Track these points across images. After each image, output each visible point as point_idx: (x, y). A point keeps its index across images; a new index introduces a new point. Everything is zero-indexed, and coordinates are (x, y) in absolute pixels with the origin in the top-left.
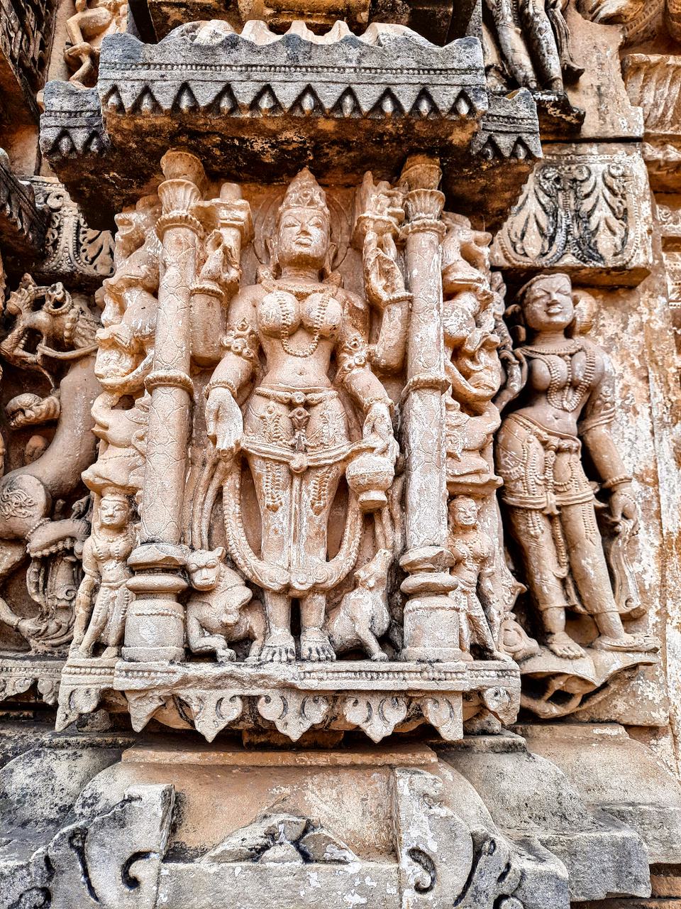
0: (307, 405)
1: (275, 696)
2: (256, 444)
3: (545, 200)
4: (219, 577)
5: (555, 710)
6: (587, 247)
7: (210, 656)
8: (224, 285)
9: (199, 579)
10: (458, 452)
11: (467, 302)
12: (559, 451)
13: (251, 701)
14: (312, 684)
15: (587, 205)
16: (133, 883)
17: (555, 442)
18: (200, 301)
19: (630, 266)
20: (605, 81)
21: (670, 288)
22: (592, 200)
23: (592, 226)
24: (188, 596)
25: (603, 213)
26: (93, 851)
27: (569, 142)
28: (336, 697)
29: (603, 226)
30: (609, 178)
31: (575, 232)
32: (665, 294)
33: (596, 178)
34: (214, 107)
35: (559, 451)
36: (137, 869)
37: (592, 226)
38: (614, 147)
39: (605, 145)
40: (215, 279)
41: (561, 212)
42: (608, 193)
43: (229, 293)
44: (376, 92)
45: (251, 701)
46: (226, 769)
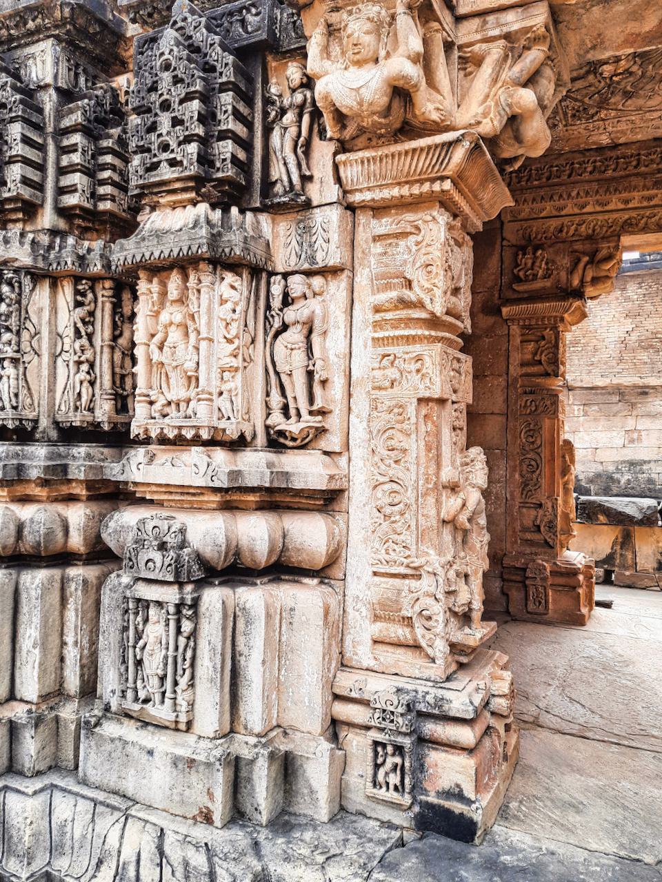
0: (175, 348)
1: (167, 427)
2: (164, 361)
3: (299, 238)
4: (158, 397)
5: (291, 444)
6: (312, 259)
7: (155, 418)
8: (154, 312)
9: (153, 398)
10: (222, 357)
11: (229, 306)
12: (292, 349)
13: (162, 429)
14: (173, 424)
15: (314, 238)
16: (139, 469)
17: (289, 346)
18: (148, 317)
19: (329, 265)
20: (324, 174)
21: (372, 263)
22: (316, 236)
23: (315, 249)
24: (151, 403)
25: (320, 241)
26: (131, 462)
27: (309, 209)
28: (180, 428)
29: (319, 248)
30: (323, 224)
31: (309, 252)
32: (369, 267)
33: (318, 224)
34: (141, 261)
35: (292, 349)
36: (140, 466)
37: (315, 249)
38: (326, 207)
39: (322, 208)
40: (151, 311)
41: (304, 244)
42: (322, 231)
43: (157, 314)
44: (178, 249)
45: (162, 429)
46: (169, 450)
